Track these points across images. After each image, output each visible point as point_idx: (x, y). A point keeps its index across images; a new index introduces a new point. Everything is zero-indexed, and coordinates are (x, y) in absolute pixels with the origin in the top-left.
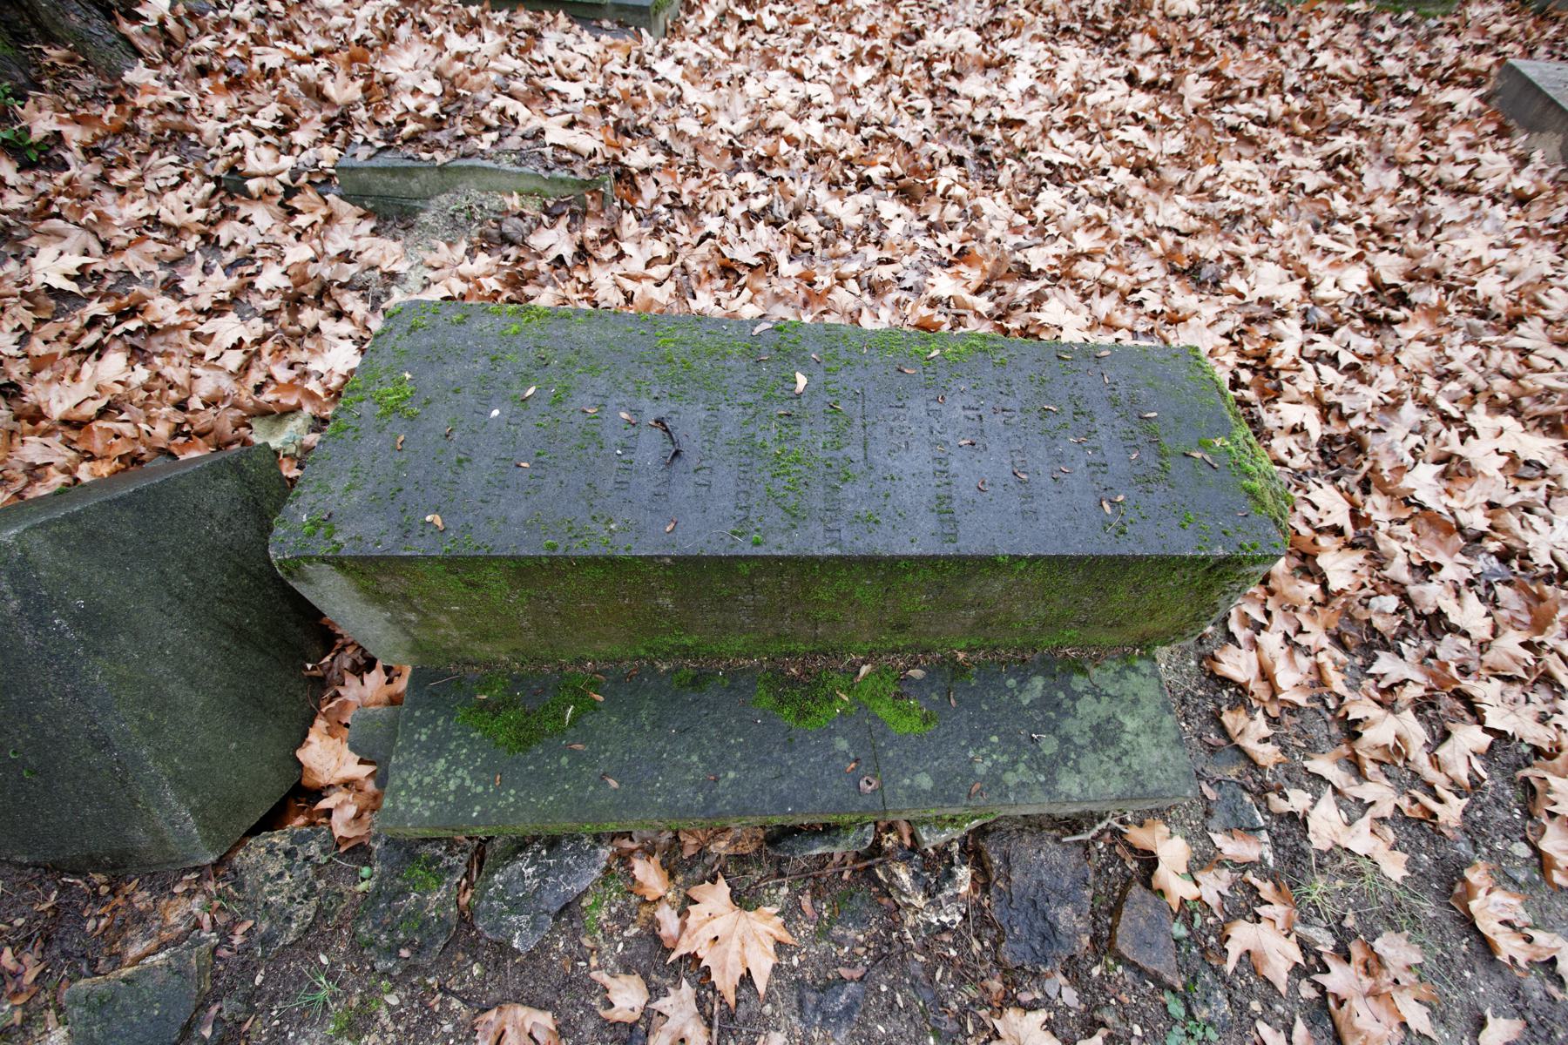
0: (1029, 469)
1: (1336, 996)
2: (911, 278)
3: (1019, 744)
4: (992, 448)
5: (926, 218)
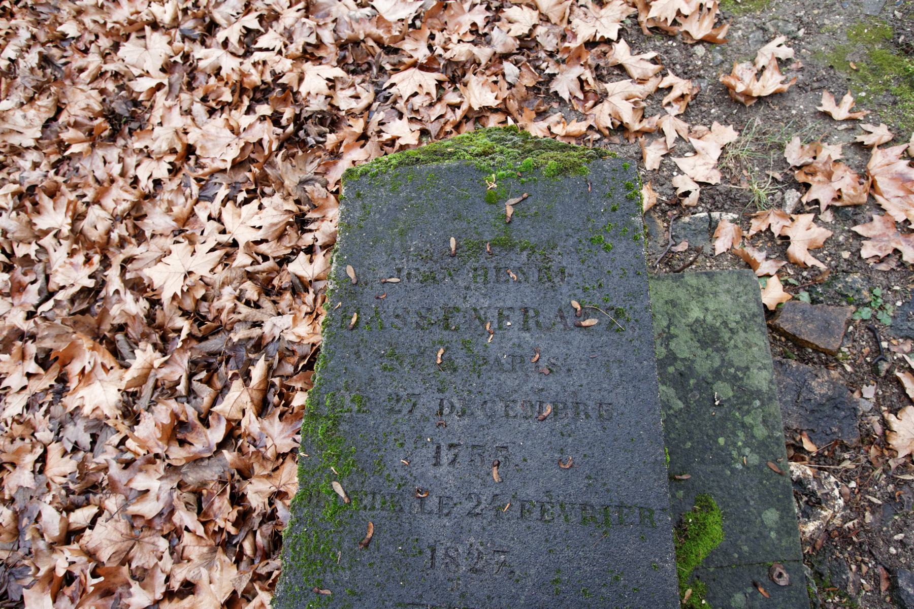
1: (834, 199)
2: (78, 433)
3: (725, 419)
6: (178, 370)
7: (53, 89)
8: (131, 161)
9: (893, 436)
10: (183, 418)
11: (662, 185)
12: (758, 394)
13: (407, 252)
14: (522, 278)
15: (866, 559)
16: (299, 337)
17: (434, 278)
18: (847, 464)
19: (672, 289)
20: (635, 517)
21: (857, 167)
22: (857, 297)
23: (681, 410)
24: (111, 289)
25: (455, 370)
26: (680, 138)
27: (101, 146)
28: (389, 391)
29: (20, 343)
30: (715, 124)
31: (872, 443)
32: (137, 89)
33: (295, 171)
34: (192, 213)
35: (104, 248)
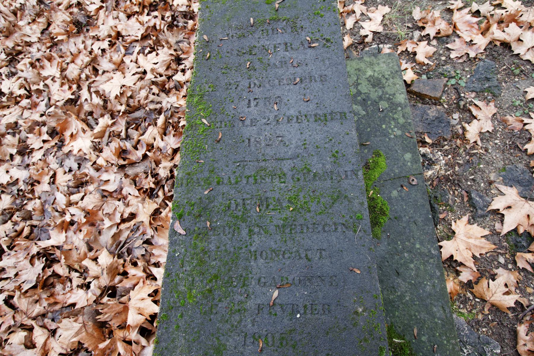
0: (292, 77)
1: (437, 33)
2: (71, 163)
3: (385, 117)
4: (278, 93)
5: (12, 156)
6: (121, 126)
7: (45, 14)
8: (89, 42)
9: (467, 133)
10: (124, 148)
11: (355, 35)
12: (400, 105)
13: (230, 27)
14: (283, 31)
15: (457, 188)
16: (180, 105)
17: (244, 36)
18: (446, 147)
19: (358, 64)
20: (338, 117)
21: (448, 20)
22: (448, 74)
23: (364, 115)
24: (83, 99)
25: (255, 70)
26: (363, 14)
27: (73, 37)
28: (226, 81)
29: (38, 127)
30: (380, 6)
31: (458, 138)
32: (90, 10)
33: (173, 36)
34: (122, 62)
35: (78, 81)
